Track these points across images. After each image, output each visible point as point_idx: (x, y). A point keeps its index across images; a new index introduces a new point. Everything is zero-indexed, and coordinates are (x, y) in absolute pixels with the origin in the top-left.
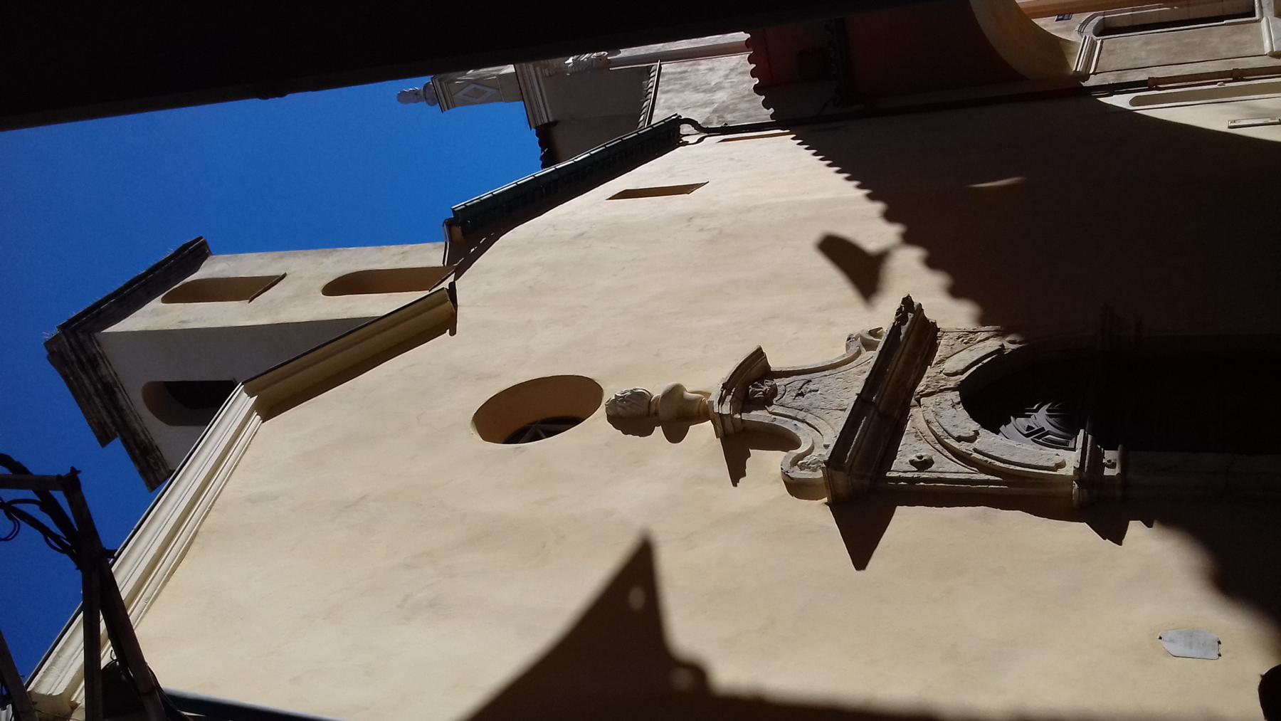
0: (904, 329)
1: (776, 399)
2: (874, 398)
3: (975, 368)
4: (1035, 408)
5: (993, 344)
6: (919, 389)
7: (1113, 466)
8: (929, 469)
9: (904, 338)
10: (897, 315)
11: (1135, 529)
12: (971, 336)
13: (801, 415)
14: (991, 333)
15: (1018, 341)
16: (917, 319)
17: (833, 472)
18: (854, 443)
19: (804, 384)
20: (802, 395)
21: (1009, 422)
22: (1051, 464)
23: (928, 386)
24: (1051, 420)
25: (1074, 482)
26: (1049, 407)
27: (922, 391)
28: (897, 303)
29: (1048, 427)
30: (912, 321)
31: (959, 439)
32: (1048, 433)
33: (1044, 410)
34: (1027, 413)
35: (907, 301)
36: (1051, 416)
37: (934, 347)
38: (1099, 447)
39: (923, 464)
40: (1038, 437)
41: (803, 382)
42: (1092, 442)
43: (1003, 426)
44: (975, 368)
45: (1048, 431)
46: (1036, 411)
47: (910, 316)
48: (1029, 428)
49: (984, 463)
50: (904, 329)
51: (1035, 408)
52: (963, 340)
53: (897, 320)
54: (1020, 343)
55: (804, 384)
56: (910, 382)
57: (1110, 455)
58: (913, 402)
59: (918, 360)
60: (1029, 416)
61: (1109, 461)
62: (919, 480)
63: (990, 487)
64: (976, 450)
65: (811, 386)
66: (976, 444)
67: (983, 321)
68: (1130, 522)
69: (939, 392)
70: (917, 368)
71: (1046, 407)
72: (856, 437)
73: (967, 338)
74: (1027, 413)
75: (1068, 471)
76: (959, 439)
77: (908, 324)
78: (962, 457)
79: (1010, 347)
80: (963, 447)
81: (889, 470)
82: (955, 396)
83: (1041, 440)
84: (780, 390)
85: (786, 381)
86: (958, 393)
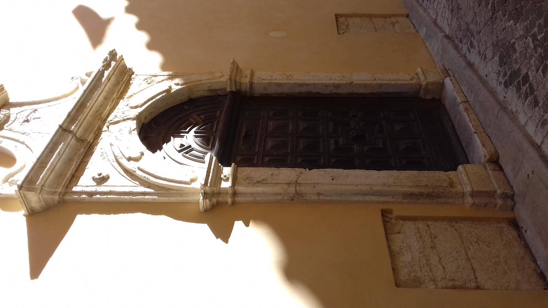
0: (106, 73)
1: (6, 125)
2: (73, 127)
3: (161, 96)
4: (187, 130)
5: (164, 86)
6: (109, 119)
7: (227, 180)
8: (105, 184)
9: (105, 80)
10: (103, 62)
11: (219, 238)
12: (153, 78)
13: (22, 138)
14: (166, 77)
15: (180, 84)
16: (118, 66)
17: (26, 193)
18: (48, 166)
19: (31, 113)
20: (27, 121)
21: (169, 140)
22: (188, 180)
23: (116, 116)
24: (197, 140)
25: (201, 194)
26: (196, 130)
27: (111, 121)
28: (106, 55)
29: (194, 146)
30: (113, 68)
31: (129, 159)
32: (192, 150)
33: (192, 132)
34: (181, 134)
35: (113, 54)
36: (196, 137)
37: (128, 84)
38: (220, 164)
39: (102, 180)
40: (187, 153)
41: (31, 111)
42: (215, 161)
43: (165, 143)
44: (161, 96)
45: (193, 148)
46: (188, 132)
47: (113, 63)
48: (182, 145)
49: (144, 179)
50: (106, 73)
51: (187, 130)
52: (147, 82)
53: (103, 66)
54: (181, 85)
55: (31, 113)
56: (106, 112)
57: (227, 171)
58: (105, 128)
59: (115, 95)
60: (182, 137)
61: (225, 176)
62: (96, 193)
63: (145, 197)
64: (139, 169)
65: (36, 115)
66: (140, 164)
67: (164, 67)
68: (236, 222)
69: (122, 121)
70: (113, 101)
71: (194, 129)
72: (52, 161)
73: (150, 79)
74: (181, 134)
75: (198, 185)
76: (129, 159)
77: (110, 69)
78: (130, 173)
79: (175, 88)
80: (131, 166)
81: (76, 185)
82: (133, 124)
83: (187, 155)
84: (12, 118)
85: (18, 109)
86: (135, 122)
